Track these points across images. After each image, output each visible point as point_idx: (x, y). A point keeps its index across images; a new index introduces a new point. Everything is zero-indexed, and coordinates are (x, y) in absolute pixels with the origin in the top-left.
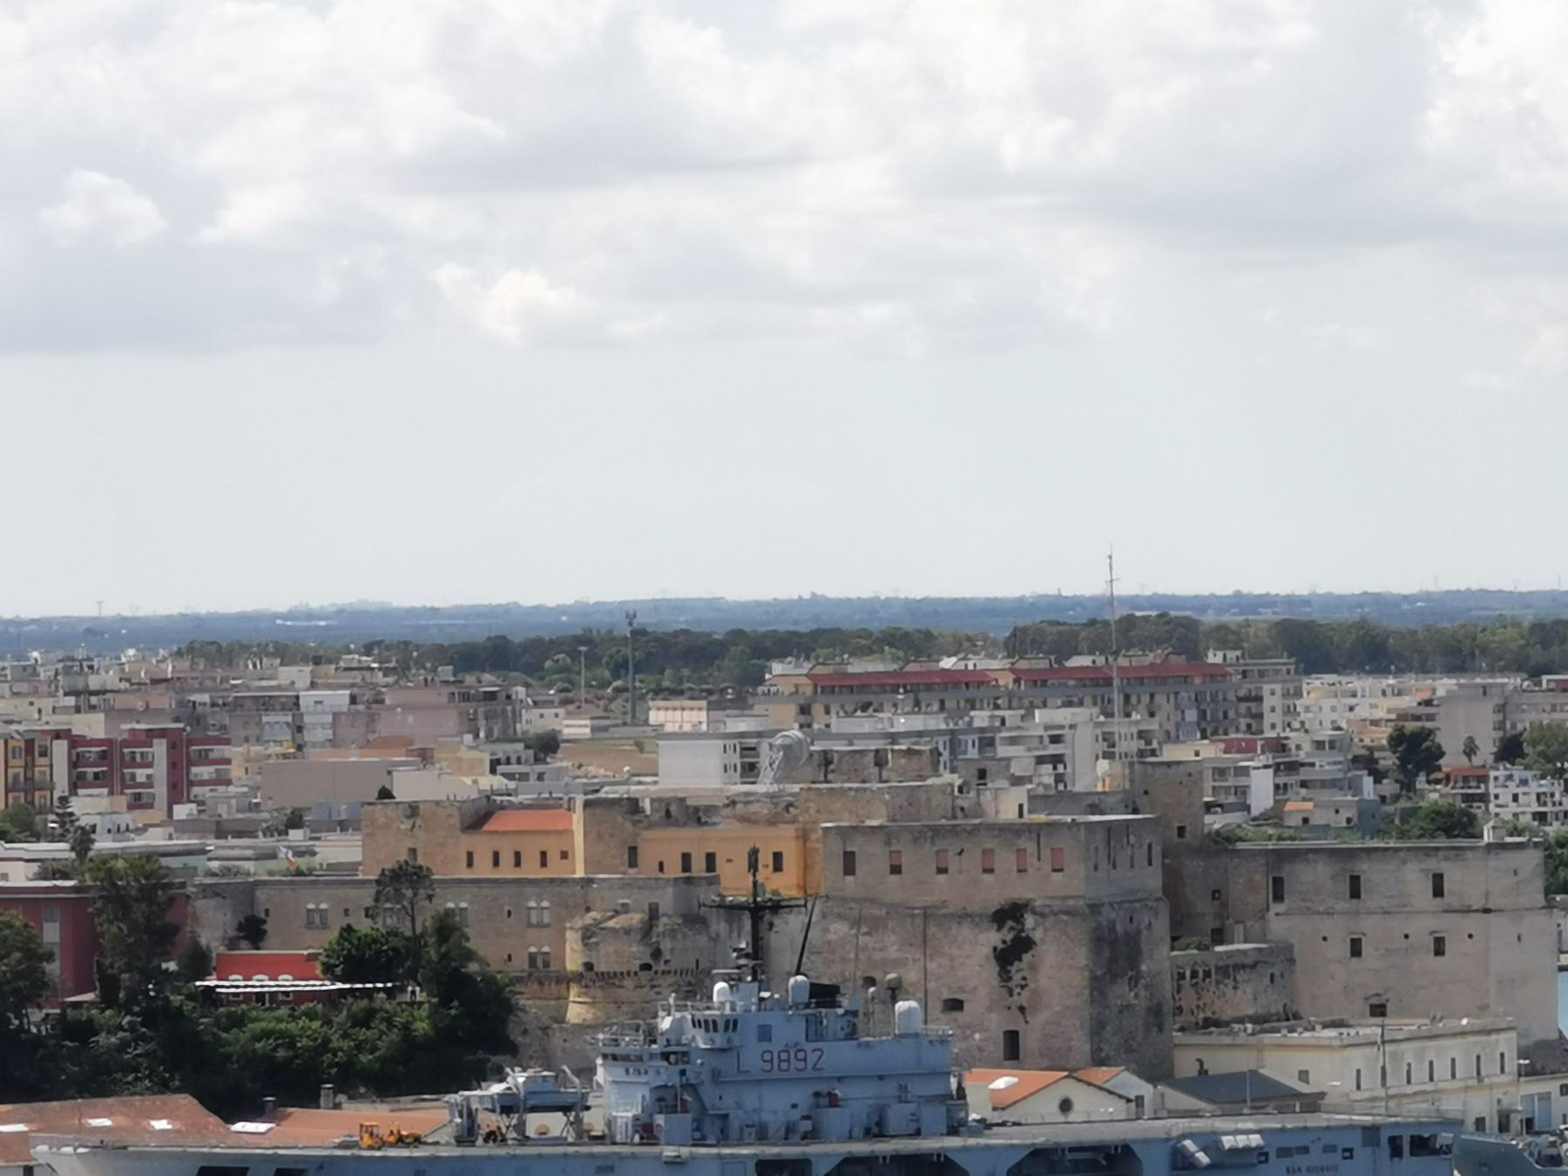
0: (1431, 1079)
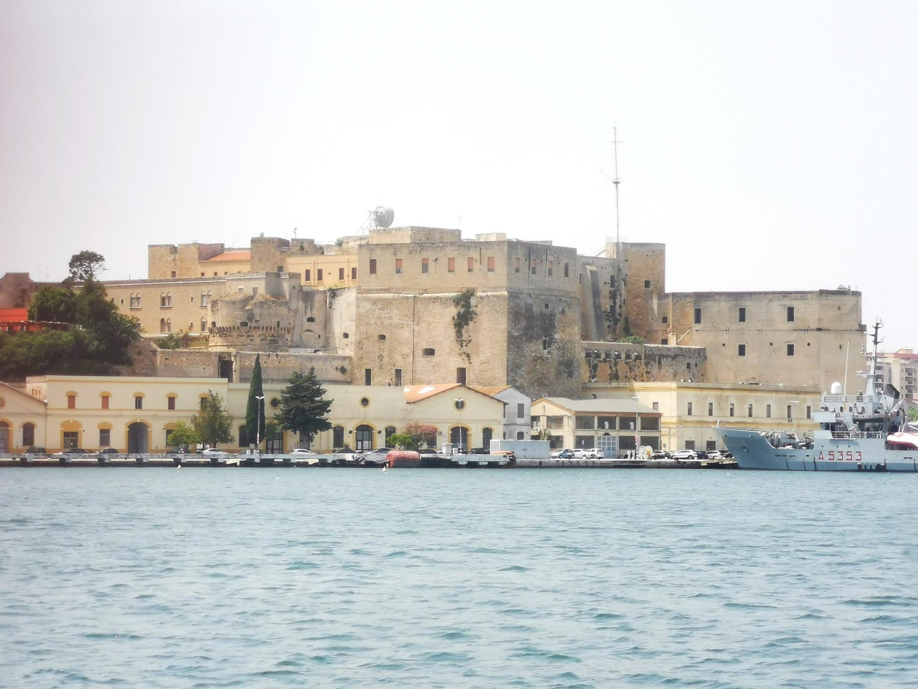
0: (750, 415)
